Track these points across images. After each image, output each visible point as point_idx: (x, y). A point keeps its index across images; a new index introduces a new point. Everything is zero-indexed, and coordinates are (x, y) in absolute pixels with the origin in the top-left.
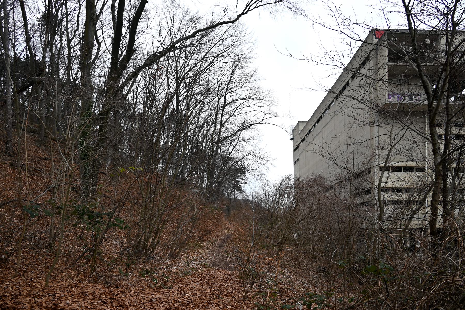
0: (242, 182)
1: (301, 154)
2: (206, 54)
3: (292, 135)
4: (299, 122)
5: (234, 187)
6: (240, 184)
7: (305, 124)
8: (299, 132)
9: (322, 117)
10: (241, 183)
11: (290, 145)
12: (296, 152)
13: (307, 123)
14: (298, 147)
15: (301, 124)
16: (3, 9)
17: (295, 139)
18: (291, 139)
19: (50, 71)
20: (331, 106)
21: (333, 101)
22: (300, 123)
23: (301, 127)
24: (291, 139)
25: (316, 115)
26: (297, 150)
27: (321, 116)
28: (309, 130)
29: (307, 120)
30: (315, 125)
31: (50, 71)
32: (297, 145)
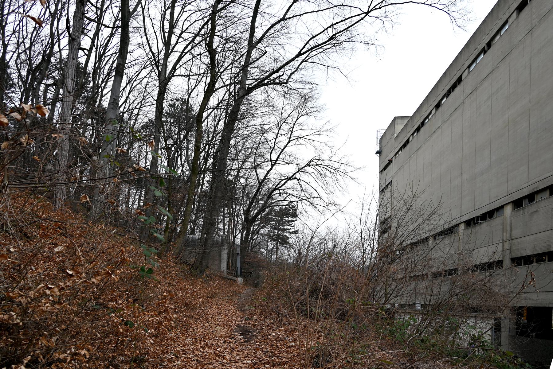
0: (291, 231)
1: (397, 173)
2: (223, 29)
3: (379, 146)
4: (395, 118)
5: (276, 240)
6: (287, 235)
7: (406, 121)
8: (395, 135)
9: (410, 140)
10: (288, 232)
11: (375, 162)
12: (384, 173)
13: (411, 118)
14: (390, 162)
15: (397, 121)
16: (47, 115)
17: (384, 153)
18: (377, 153)
19: (226, 233)
20: (426, 121)
21: (430, 113)
22: (396, 120)
23: (399, 127)
24: (377, 153)
25: (446, 81)
26: (389, 168)
27: (409, 139)
28: (421, 120)
29: (411, 114)
30: (438, 106)
31: (226, 233)
32: (390, 159)
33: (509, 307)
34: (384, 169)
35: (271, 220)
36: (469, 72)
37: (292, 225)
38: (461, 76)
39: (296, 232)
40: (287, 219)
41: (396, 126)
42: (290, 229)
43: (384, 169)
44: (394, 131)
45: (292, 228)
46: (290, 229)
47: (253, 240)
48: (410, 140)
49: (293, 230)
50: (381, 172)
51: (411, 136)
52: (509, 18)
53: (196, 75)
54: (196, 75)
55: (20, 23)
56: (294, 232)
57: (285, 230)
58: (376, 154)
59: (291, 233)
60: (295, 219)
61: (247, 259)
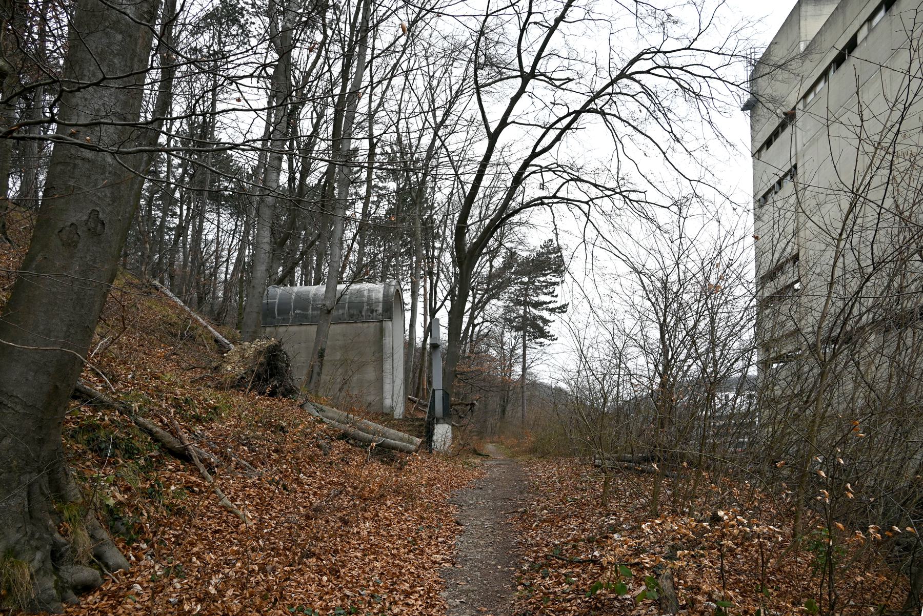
0: (551, 306)
6: (546, 314)
33: (383, 149)
34: (768, 143)
35: (509, 282)
36: (870, 30)
37: (553, 292)
38: (855, 37)
39: (563, 309)
40: (542, 279)
41: (802, 23)
42: (550, 302)
43: (768, 143)
44: (799, 36)
45: (553, 299)
46: (550, 302)
47: (475, 326)
48: (860, 38)
49: (558, 305)
50: (757, 154)
51: (865, 28)
52: (858, 31)
53: (567, 201)
54: (567, 201)
55: (315, 80)
56: (559, 308)
57: (537, 305)
58: (743, 110)
59: (552, 310)
60: (558, 280)
61: (462, 367)
